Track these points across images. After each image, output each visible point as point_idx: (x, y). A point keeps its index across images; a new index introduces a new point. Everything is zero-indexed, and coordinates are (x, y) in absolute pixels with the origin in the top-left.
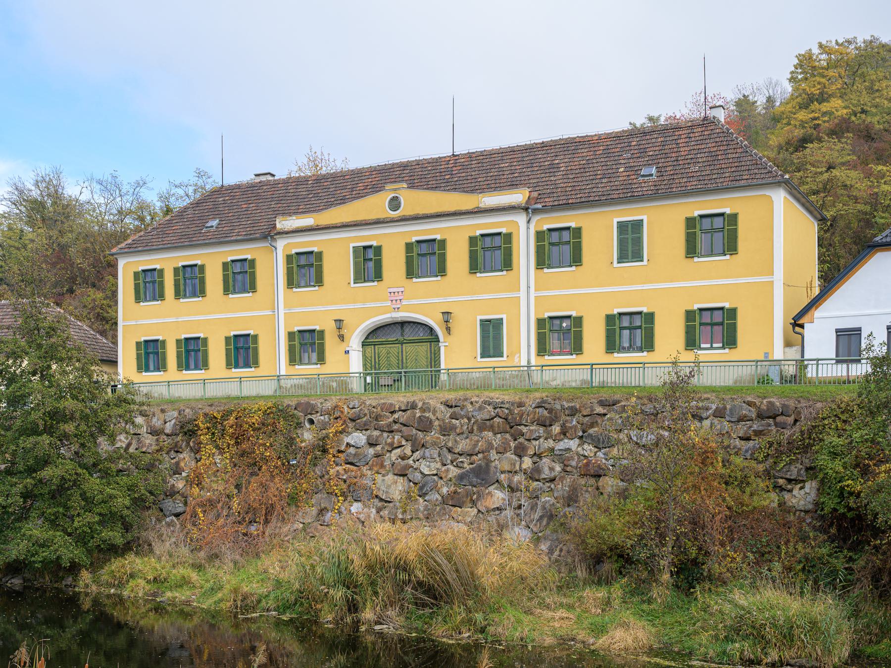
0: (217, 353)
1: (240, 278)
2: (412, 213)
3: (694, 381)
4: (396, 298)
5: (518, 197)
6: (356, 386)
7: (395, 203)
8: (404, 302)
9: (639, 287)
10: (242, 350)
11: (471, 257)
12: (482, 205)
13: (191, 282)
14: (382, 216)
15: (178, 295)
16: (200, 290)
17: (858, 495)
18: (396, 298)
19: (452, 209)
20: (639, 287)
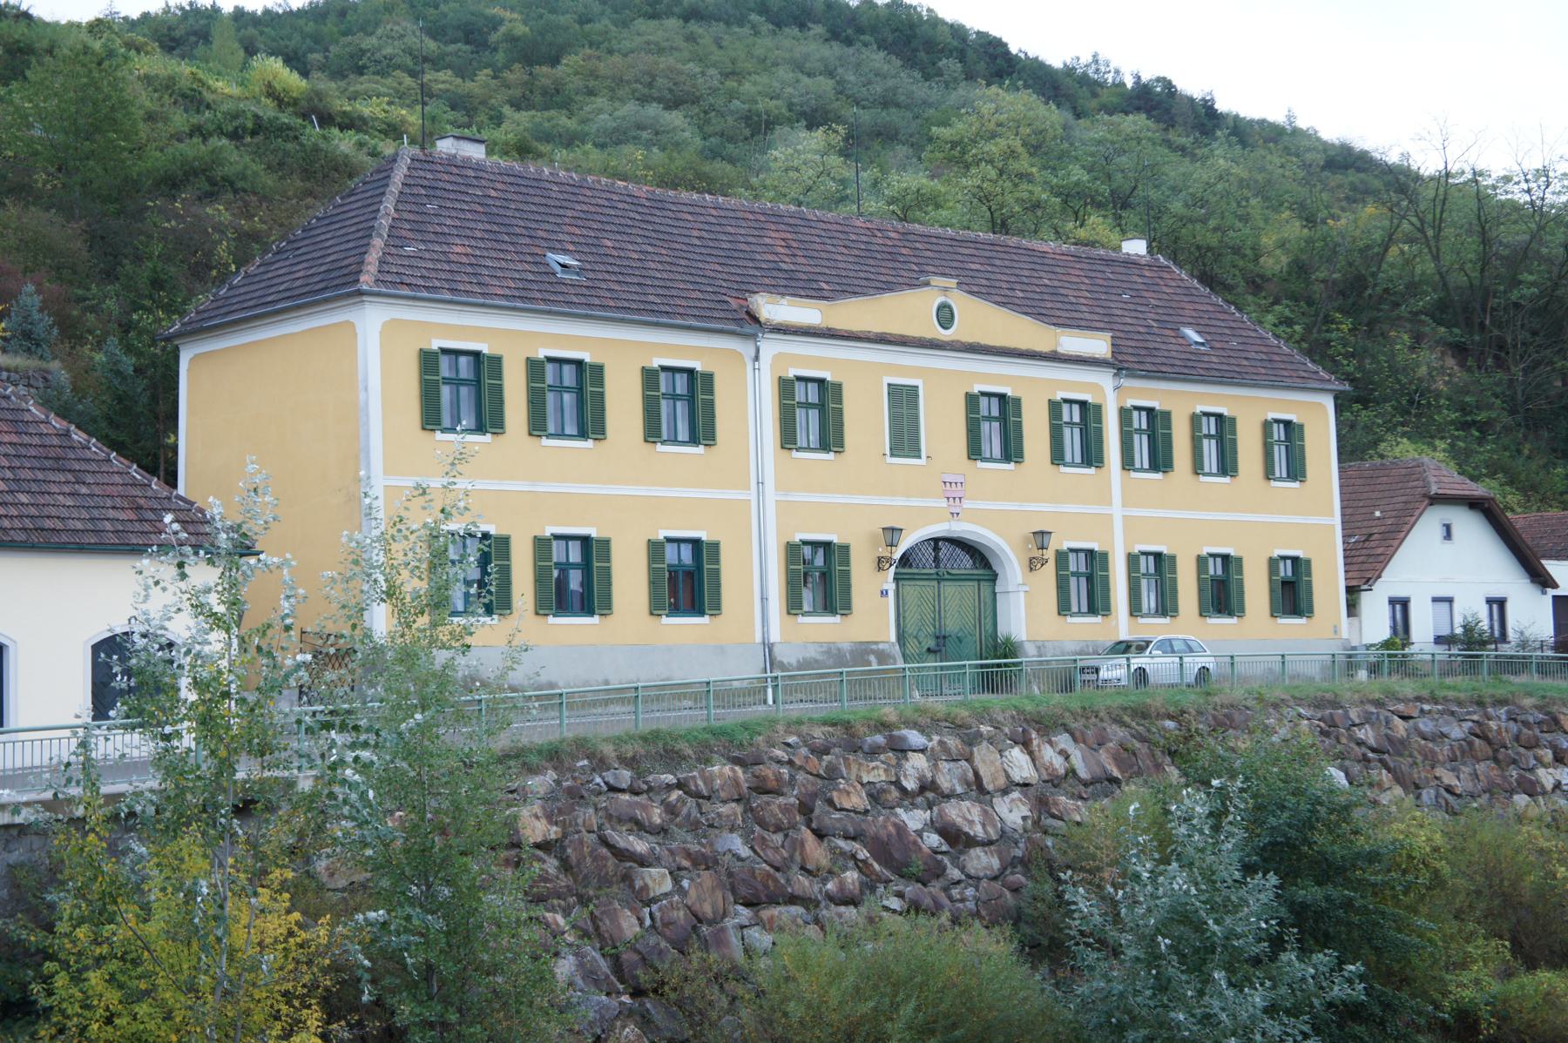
0: (630, 579)
1: (684, 409)
2: (917, 335)
3: (516, 677)
4: (953, 492)
5: (1098, 345)
6: (1317, 678)
7: (945, 316)
8: (967, 504)
9: (1161, 513)
10: (687, 582)
11: (1052, 437)
12: (1061, 350)
13: (573, 401)
14: (928, 335)
15: (537, 425)
16: (591, 424)
17: (50, 993)
18: (953, 492)
19: (1023, 345)
20: (1161, 513)
